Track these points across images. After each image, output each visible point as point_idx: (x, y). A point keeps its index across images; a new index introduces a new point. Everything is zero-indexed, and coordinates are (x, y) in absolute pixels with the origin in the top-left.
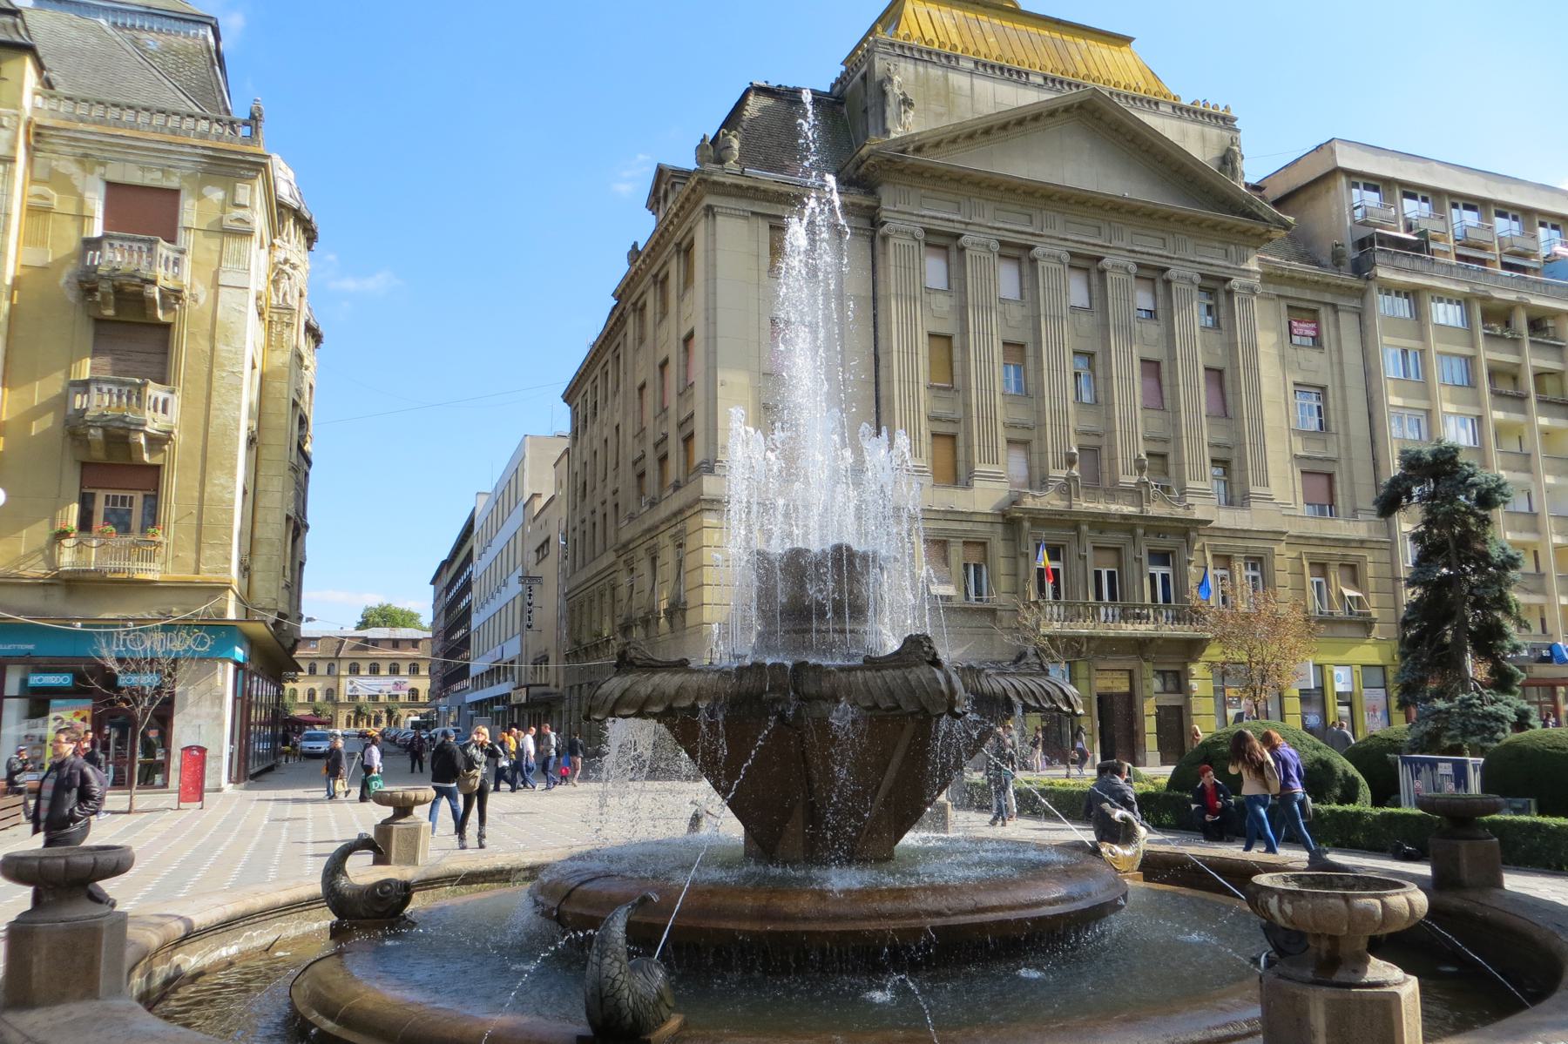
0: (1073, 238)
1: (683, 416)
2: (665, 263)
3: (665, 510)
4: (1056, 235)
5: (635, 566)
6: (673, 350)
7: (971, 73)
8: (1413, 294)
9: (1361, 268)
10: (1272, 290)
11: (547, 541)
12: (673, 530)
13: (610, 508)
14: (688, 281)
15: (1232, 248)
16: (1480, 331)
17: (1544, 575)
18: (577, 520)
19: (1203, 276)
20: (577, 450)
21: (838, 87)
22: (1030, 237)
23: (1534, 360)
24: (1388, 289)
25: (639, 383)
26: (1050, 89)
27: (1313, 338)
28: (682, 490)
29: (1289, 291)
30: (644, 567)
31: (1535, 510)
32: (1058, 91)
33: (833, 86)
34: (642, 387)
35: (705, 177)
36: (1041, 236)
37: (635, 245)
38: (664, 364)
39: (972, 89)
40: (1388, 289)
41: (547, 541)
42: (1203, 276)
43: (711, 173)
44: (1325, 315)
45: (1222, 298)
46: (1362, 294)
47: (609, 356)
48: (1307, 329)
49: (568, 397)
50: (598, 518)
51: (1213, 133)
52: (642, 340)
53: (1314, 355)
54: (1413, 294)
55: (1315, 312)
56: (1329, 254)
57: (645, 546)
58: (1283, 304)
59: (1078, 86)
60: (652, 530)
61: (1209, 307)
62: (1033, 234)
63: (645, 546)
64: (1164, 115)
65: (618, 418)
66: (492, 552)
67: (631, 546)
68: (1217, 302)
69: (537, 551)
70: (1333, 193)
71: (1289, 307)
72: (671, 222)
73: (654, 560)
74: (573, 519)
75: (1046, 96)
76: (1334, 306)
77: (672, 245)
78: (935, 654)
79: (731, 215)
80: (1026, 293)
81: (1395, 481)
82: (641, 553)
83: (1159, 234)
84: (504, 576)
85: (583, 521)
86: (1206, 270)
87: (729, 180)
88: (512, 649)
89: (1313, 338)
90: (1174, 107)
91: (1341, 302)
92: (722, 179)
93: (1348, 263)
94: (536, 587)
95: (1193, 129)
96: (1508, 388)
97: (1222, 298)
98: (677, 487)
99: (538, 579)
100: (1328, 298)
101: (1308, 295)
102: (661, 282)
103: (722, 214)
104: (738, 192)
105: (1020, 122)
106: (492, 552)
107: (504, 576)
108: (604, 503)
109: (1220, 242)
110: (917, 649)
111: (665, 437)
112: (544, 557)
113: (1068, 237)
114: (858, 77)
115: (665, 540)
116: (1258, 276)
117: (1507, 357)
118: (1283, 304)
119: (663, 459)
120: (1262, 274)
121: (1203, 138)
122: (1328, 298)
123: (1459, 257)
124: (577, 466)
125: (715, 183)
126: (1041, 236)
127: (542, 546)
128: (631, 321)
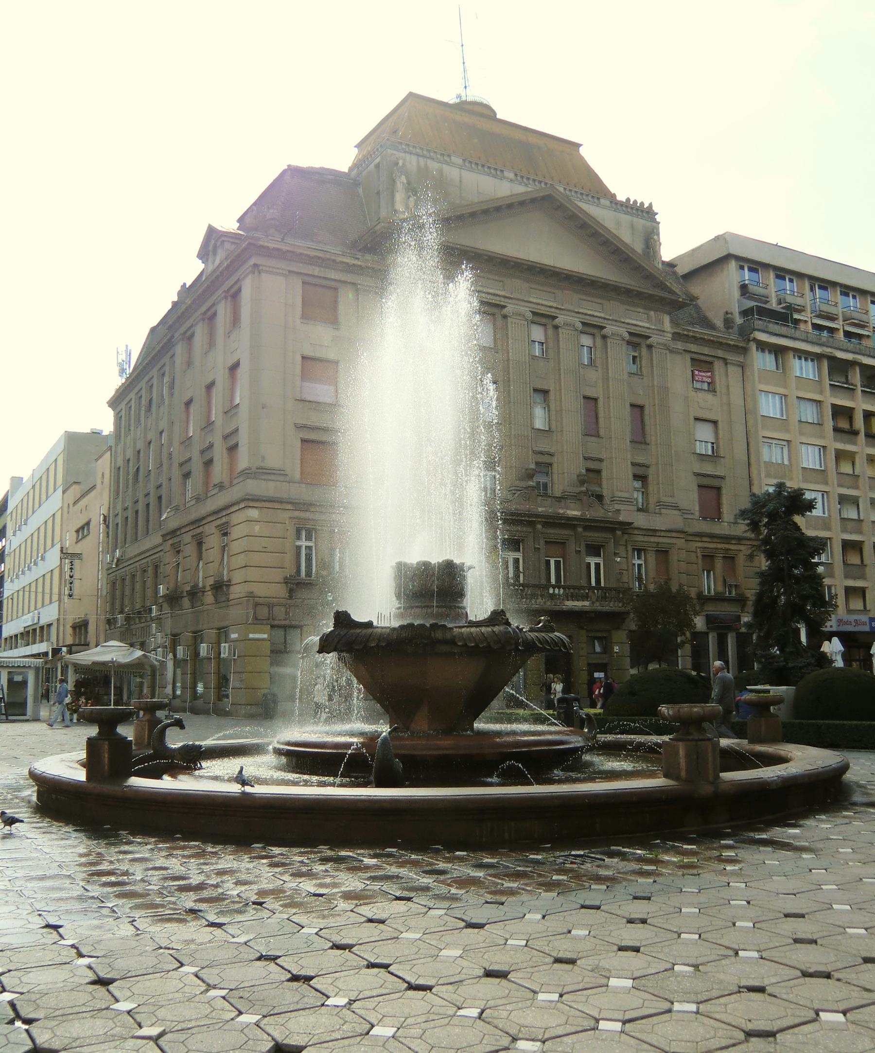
0: (535, 301)
1: (228, 431)
2: (214, 305)
3: (210, 506)
4: (522, 298)
5: (181, 548)
6: (221, 376)
7: (461, 168)
8: (779, 351)
9: (745, 333)
10: (680, 345)
11: (88, 524)
12: (219, 522)
13: (152, 499)
14: (236, 320)
15: (652, 313)
16: (827, 382)
17: (866, 566)
18: (119, 508)
19: (630, 334)
20: (120, 449)
21: (355, 171)
22: (502, 299)
23: (861, 404)
24: (763, 346)
25: (186, 398)
26: (520, 184)
27: (709, 383)
28: (225, 491)
29: (693, 347)
30: (190, 550)
31: (862, 518)
32: (526, 185)
33: (351, 169)
34: (188, 403)
35: (253, 241)
36: (510, 298)
37: (185, 284)
38: (210, 386)
39: (461, 178)
40: (763, 346)
41: (88, 524)
42: (630, 334)
43: (258, 239)
44: (718, 366)
45: (644, 351)
46: (744, 351)
47: (154, 372)
48: (705, 376)
49: (114, 403)
50: (141, 506)
51: (640, 223)
52: (189, 364)
53: (709, 396)
54: (779, 351)
55: (711, 363)
56: (722, 319)
57: (191, 533)
58: (688, 357)
59: (540, 182)
60: (198, 522)
61: (634, 358)
62: (505, 297)
63: (191, 533)
64: (604, 207)
65: (163, 424)
66: (27, 531)
67: (178, 533)
68: (640, 354)
69: (77, 531)
70: (725, 273)
71: (692, 359)
72: (222, 273)
73: (200, 544)
74: (115, 507)
75: (520, 189)
76: (725, 359)
77: (220, 292)
78: (508, 619)
79: (272, 273)
80: (499, 343)
81: (760, 596)
82: (187, 538)
83: (599, 301)
84: (41, 551)
85: (126, 509)
86: (633, 329)
87: (272, 245)
88: (49, 614)
89: (709, 383)
90: (611, 202)
91: (730, 357)
92: (266, 244)
93: (736, 328)
94: (77, 562)
95: (625, 218)
96: (844, 424)
97: (644, 351)
98: (221, 487)
99: (78, 556)
100: (720, 353)
101: (706, 350)
102: (211, 318)
103: (267, 272)
104: (280, 254)
105: (498, 209)
106: (27, 531)
107: (41, 551)
108: (147, 495)
109: (645, 308)
110: (497, 617)
111: (211, 446)
112: (84, 537)
113: (531, 300)
114: (372, 166)
115: (210, 529)
116: (670, 335)
117: (843, 401)
118: (688, 357)
119: (209, 463)
120: (674, 334)
121: (632, 227)
122: (720, 353)
123: (816, 326)
124: (120, 462)
125: (262, 246)
126: (510, 298)
127: (82, 528)
128: (179, 349)
